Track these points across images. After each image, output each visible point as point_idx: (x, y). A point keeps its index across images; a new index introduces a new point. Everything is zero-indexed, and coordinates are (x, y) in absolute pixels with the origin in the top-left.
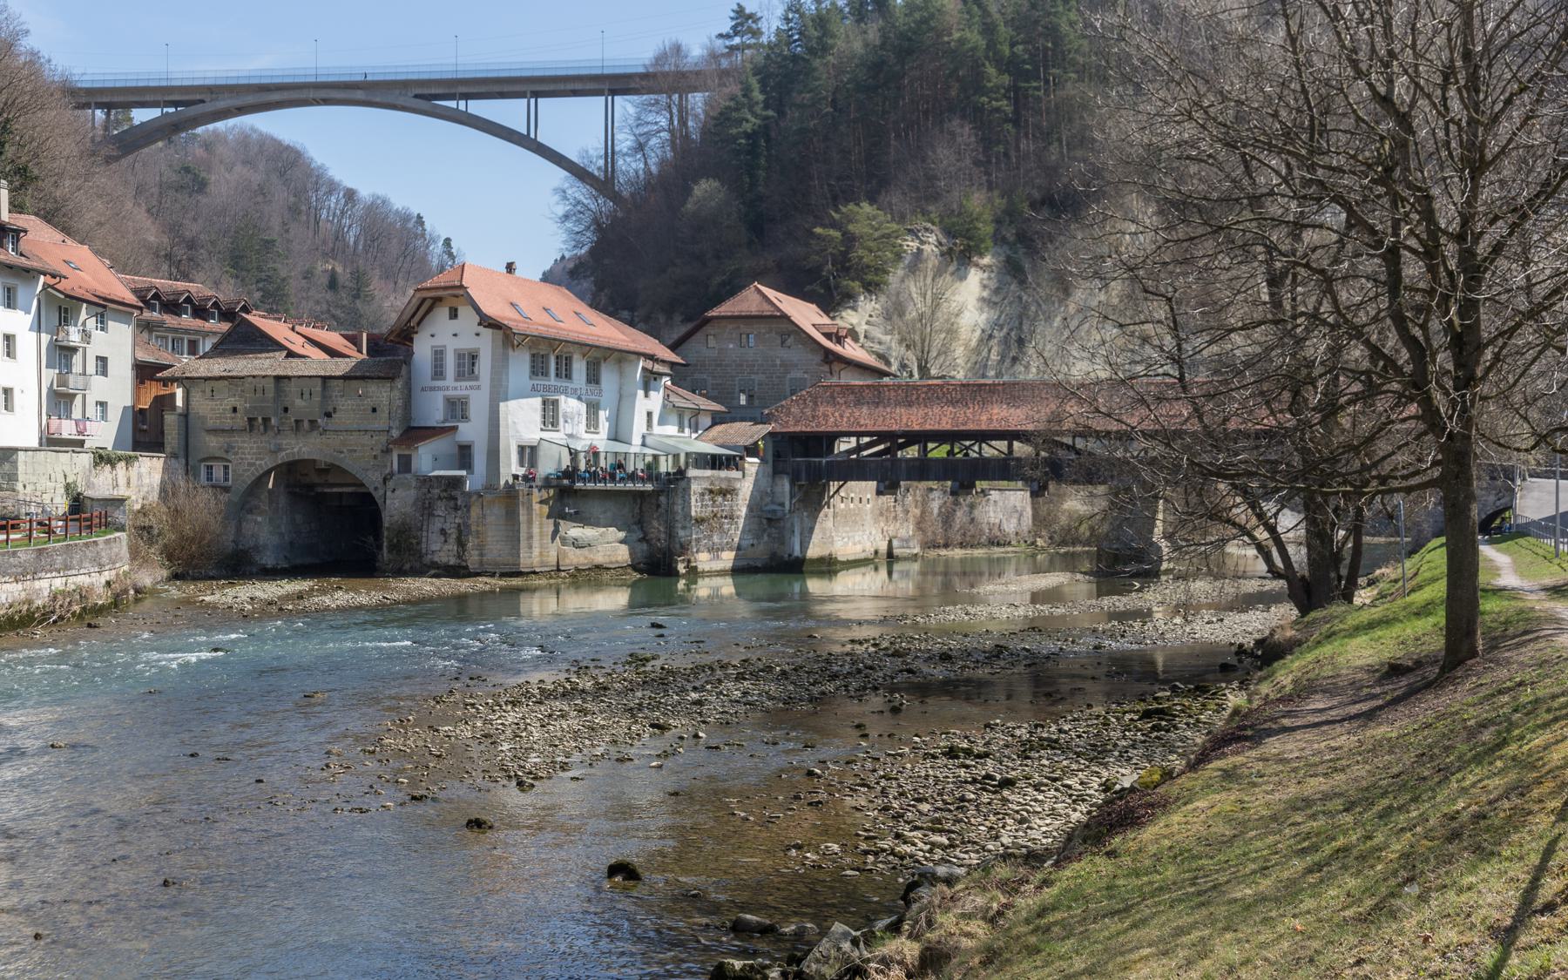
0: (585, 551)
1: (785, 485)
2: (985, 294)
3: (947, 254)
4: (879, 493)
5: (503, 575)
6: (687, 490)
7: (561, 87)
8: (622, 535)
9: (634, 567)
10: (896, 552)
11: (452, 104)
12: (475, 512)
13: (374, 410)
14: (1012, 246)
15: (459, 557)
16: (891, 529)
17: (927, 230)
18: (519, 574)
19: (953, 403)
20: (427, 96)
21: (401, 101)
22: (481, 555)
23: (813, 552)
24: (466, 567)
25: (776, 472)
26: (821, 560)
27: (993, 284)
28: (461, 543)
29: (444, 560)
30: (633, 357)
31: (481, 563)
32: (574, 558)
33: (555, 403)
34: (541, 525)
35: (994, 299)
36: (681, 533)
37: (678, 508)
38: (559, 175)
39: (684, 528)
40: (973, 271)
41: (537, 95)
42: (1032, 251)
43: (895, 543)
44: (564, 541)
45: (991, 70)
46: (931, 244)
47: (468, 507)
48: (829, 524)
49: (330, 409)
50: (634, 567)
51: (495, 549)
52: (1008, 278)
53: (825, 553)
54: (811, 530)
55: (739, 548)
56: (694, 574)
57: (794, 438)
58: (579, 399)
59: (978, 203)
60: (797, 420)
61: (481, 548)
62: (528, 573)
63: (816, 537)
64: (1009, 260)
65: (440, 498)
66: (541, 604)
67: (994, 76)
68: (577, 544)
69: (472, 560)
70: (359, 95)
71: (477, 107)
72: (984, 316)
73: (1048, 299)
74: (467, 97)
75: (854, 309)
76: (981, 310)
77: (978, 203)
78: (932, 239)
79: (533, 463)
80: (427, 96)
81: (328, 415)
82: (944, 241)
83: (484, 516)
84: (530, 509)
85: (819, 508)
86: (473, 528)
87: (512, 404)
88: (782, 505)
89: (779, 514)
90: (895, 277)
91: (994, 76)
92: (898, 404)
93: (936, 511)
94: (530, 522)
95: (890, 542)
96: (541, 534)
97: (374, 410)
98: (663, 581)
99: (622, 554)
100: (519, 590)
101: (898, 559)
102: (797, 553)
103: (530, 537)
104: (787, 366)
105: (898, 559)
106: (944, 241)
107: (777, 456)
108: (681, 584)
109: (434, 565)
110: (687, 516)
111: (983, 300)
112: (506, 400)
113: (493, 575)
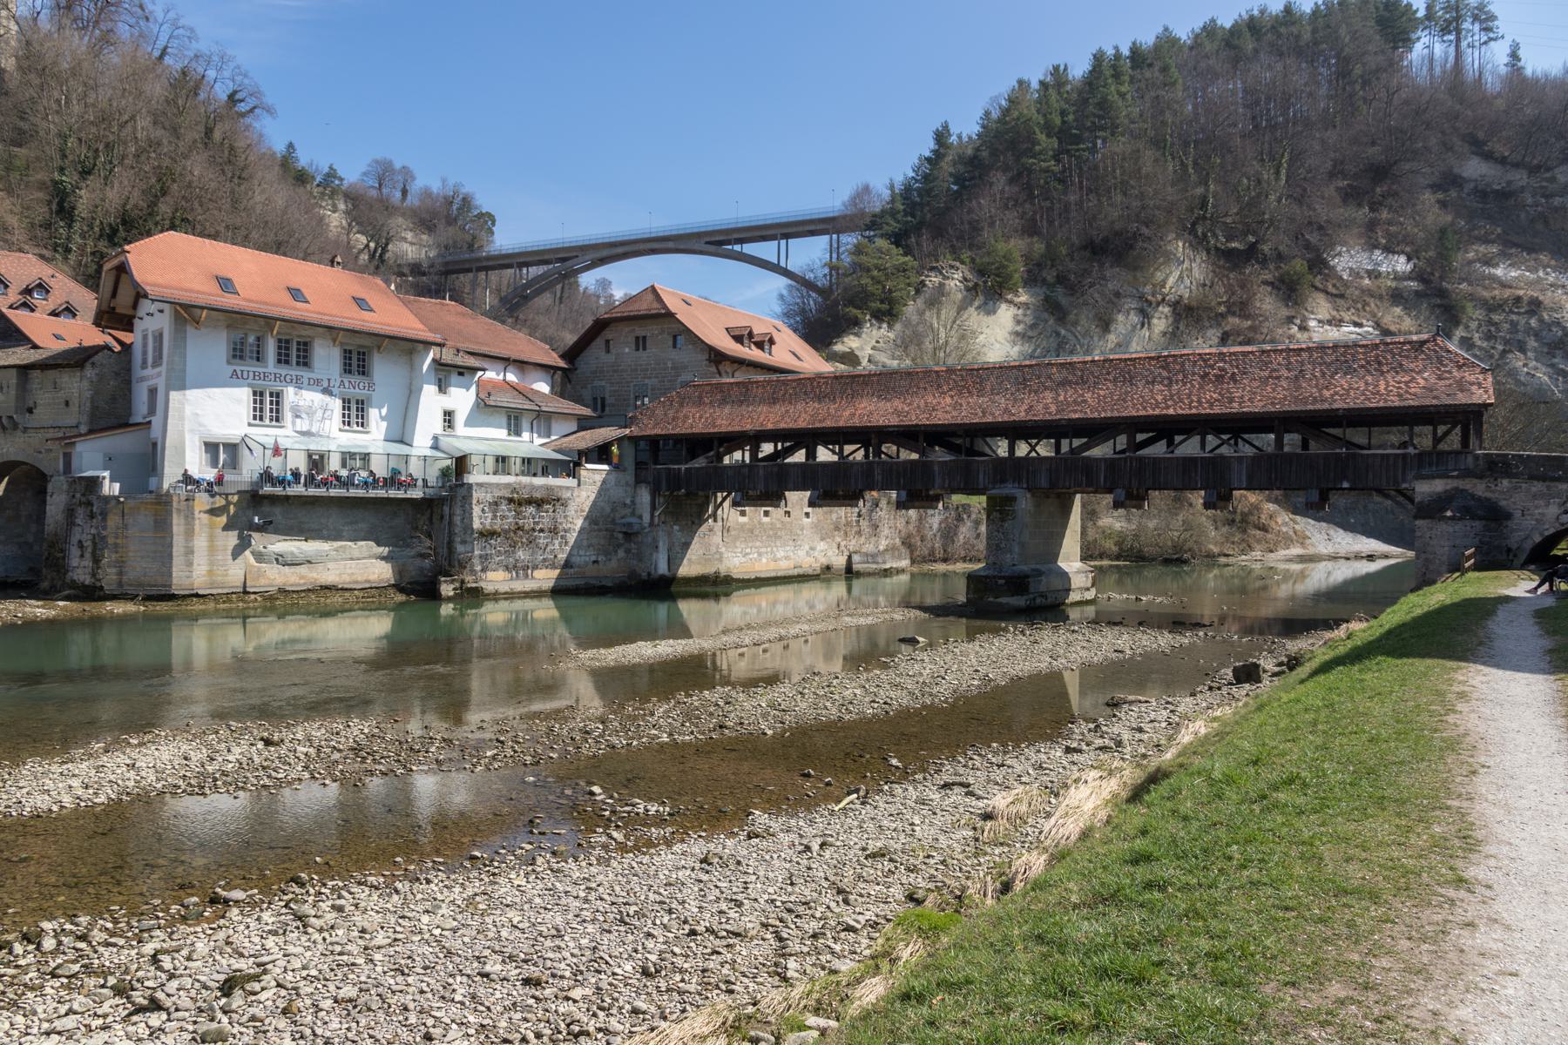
0: (303, 570)
1: (644, 496)
2: (1019, 328)
3: (972, 290)
4: (812, 504)
5: (149, 598)
6: (467, 498)
7: (801, 229)
8: (384, 550)
9: (398, 587)
10: (856, 567)
11: (737, 248)
12: (113, 521)
13: (67, 403)
14: (1051, 286)
15: (94, 575)
16: (853, 544)
17: (952, 267)
18: (171, 597)
19: (820, 398)
20: (718, 242)
21: (696, 247)
22: (120, 573)
23: (686, 569)
24: (101, 588)
25: (638, 481)
26: (702, 580)
27: (1029, 320)
28: (96, 560)
29: (82, 578)
30: (421, 347)
31: (120, 584)
32: (276, 577)
33: (277, 397)
34: (211, 538)
35: (1030, 333)
36: (460, 548)
37: (457, 520)
38: (781, 282)
39: (464, 542)
40: (1004, 306)
41: (787, 236)
42: (1072, 290)
43: (856, 558)
44: (259, 557)
45: (1042, 137)
46: (955, 281)
47: (104, 515)
48: (717, 539)
49: (31, 404)
50: (398, 587)
51: (139, 568)
52: (1046, 315)
53: (709, 570)
54: (687, 545)
55: (567, 564)
56: (473, 596)
57: (654, 442)
58: (327, 391)
59: (1014, 248)
60: (659, 421)
61: (120, 565)
62: (184, 597)
63: (695, 550)
64: (1047, 299)
65: (80, 504)
66: (210, 640)
67: (1045, 142)
68: (281, 560)
69: (109, 578)
70: (671, 245)
71: (749, 249)
72: (1016, 349)
73: (1087, 334)
74: (741, 241)
75: (857, 335)
76: (1015, 344)
77: (1014, 248)
78: (958, 275)
79: (233, 463)
80: (718, 242)
81: (30, 411)
82: (969, 276)
83: (125, 527)
84: (189, 517)
85: (700, 521)
86: (111, 541)
87: (192, 394)
88: (640, 517)
89: (636, 528)
90: (910, 309)
91: (1045, 142)
92: (762, 401)
93: (935, 526)
94: (189, 533)
95: (850, 557)
96: (212, 549)
97: (67, 403)
98: (431, 604)
99: (382, 572)
100: (168, 619)
101: (859, 574)
102: (663, 568)
103: (190, 551)
104: (678, 368)
105: (859, 574)
106: (969, 276)
107: (640, 465)
108: (447, 610)
109: (74, 585)
110: (468, 527)
111: (1017, 334)
112: (182, 387)
113: (132, 598)
